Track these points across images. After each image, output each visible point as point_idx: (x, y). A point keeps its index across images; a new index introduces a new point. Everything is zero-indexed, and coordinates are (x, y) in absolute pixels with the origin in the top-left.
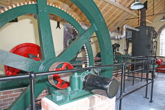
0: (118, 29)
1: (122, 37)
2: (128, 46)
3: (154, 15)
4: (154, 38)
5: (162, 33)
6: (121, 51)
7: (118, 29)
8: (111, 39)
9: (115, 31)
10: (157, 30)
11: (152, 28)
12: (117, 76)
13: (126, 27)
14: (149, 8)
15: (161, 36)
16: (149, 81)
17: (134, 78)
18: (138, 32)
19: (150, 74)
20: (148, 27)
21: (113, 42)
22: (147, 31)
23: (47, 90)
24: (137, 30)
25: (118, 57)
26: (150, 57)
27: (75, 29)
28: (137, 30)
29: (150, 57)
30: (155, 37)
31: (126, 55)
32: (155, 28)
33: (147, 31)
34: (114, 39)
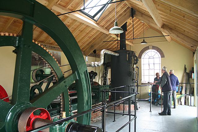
0: (95, 52)
1: (100, 65)
2: (106, 70)
3: (134, 39)
4: (135, 64)
5: (142, 57)
6: (98, 80)
7: (95, 52)
8: (87, 66)
9: (91, 55)
10: (137, 55)
11: (133, 52)
12: (95, 112)
13: (104, 52)
14: (128, 29)
15: (142, 60)
16: (132, 117)
17: (115, 112)
18: (118, 56)
19: (132, 106)
20: (128, 51)
21: (89, 70)
22: (127, 56)
23: (73, 119)
24: (117, 55)
25: (95, 87)
26: (124, 111)
27: (41, 57)
28: (117, 55)
29: (124, 111)
30: (136, 62)
31: (104, 86)
32: (135, 52)
33: (127, 56)
34: (90, 66)
